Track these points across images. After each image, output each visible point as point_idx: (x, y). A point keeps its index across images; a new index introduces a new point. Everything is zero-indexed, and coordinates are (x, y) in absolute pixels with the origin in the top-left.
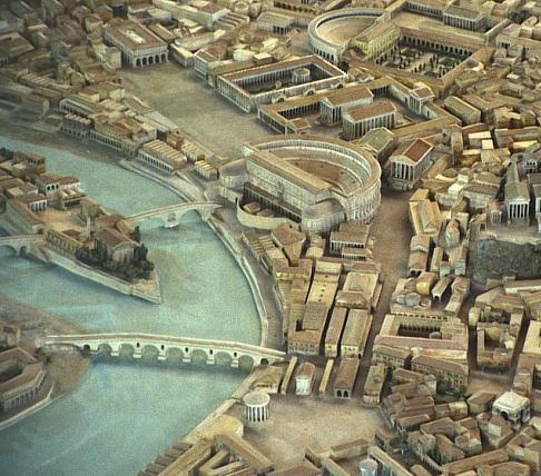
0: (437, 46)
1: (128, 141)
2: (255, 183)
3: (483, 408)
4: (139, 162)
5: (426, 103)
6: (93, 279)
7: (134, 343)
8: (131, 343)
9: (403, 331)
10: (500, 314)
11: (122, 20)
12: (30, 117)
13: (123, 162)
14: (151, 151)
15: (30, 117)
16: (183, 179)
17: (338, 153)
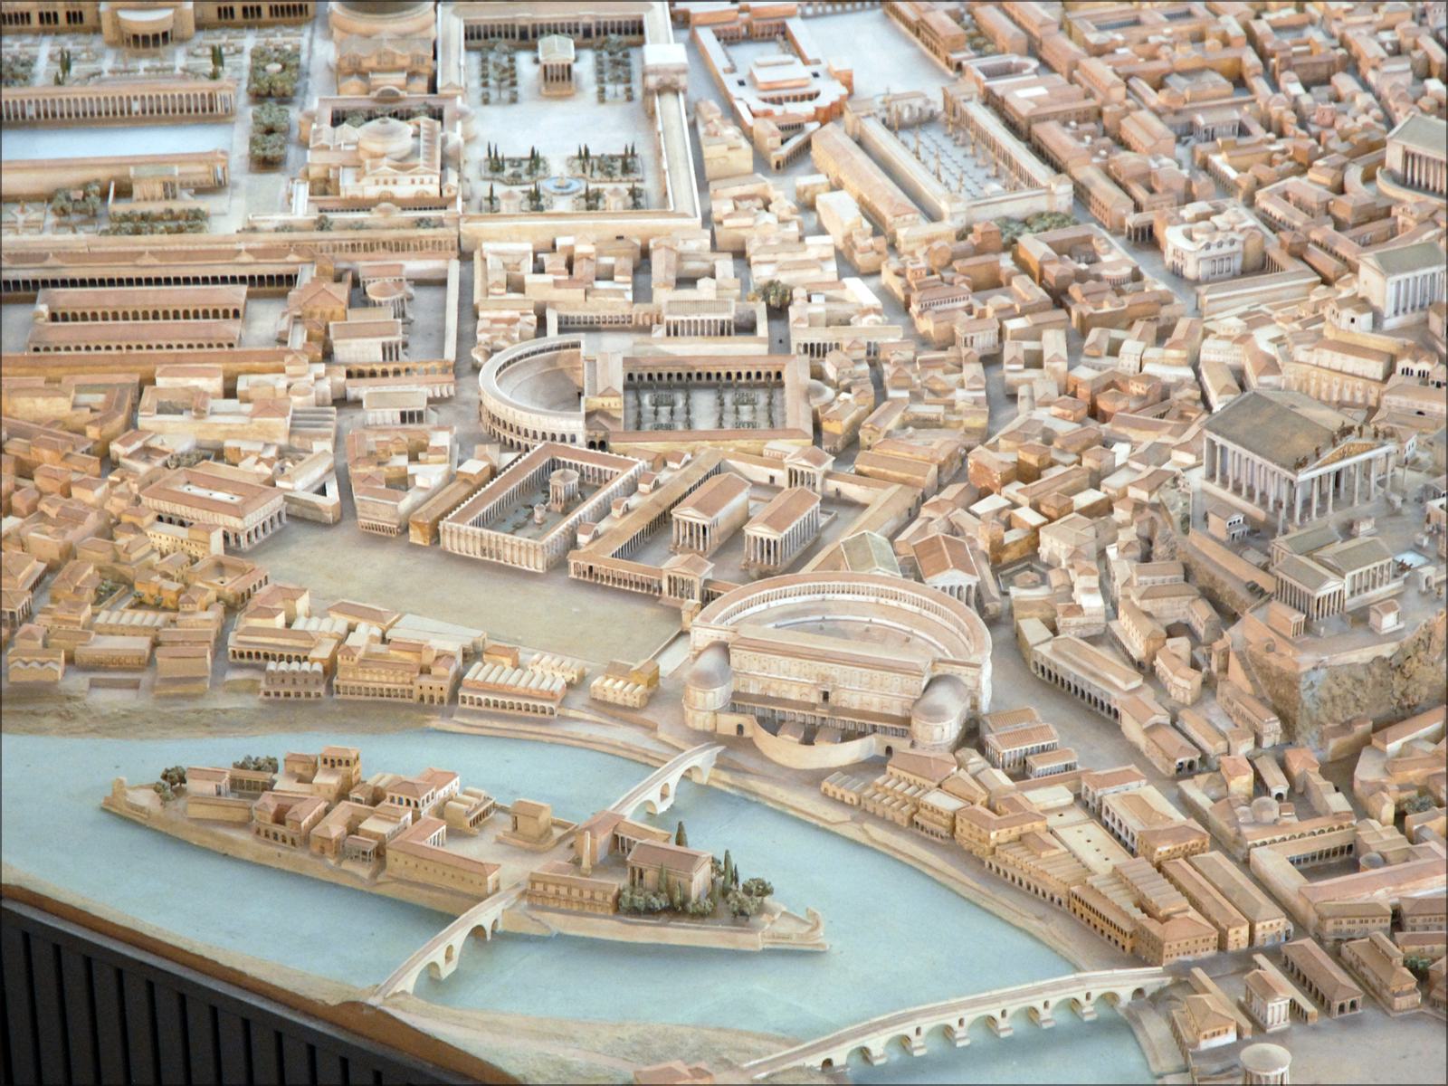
0: (699, 375)
1: (425, 681)
2: (754, 690)
3: (628, 264)
4: (465, 713)
5: (828, 475)
6: (672, 942)
7: (908, 1029)
8: (904, 1032)
9: (933, 216)
10: (1414, 793)
11: (22, 456)
12: (194, 689)
13: (436, 722)
14: (484, 687)
15: (194, 689)
16: (577, 720)
17: (932, 616)
